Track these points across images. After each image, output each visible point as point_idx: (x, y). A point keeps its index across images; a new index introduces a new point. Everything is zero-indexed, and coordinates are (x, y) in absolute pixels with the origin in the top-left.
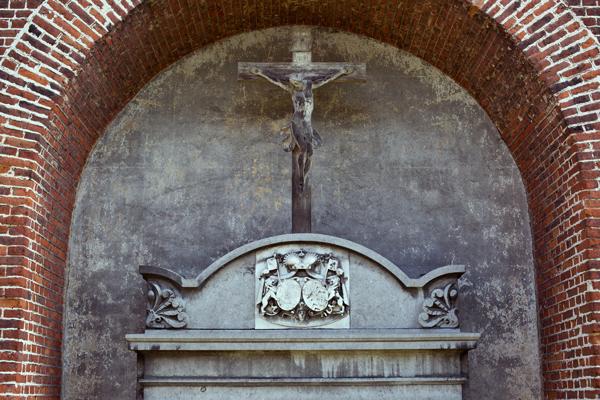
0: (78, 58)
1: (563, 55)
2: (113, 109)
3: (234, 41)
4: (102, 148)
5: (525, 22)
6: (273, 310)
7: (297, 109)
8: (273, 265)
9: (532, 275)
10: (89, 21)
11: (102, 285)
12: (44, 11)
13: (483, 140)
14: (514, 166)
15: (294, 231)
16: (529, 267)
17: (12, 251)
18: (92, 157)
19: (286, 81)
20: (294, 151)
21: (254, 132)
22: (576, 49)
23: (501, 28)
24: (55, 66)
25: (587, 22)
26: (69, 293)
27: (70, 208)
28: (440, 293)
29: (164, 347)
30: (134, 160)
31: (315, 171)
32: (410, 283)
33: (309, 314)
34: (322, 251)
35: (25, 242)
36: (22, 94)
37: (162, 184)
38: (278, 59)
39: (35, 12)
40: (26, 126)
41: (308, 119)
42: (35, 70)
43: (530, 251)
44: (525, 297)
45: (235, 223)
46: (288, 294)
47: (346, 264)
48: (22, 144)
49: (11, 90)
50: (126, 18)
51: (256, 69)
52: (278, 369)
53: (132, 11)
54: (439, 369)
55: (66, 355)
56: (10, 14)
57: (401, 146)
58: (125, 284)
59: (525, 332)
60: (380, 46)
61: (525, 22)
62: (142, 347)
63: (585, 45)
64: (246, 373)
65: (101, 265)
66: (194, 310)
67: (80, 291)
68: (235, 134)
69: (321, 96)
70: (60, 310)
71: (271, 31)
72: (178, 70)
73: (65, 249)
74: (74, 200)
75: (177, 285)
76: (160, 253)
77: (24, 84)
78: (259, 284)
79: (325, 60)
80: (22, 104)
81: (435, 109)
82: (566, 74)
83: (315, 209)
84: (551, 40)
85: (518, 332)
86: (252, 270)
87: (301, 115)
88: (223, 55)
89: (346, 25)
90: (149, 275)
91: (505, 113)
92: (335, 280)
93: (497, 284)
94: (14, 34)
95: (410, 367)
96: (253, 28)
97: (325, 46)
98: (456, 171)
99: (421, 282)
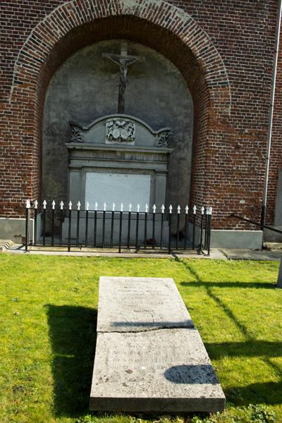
0: (50, 49)
1: (209, 62)
2: (58, 66)
3: (100, 44)
4: (54, 80)
5: (199, 49)
6: (112, 138)
7: (122, 72)
8: (112, 123)
9: (192, 132)
10: (53, 35)
11: (55, 127)
12: (36, 29)
13: (181, 87)
14: (190, 96)
15: (118, 113)
16: (191, 130)
17: (29, 115)
18: (51, 83)
19: (118, 61)
20: (120, 86)
21: (106, 78)
22: (214, 60)
23: (191, 50)
24: (42, 51)
25: (219, 51)
26: (44, 129)
27: (44, 100)
28: (163, 136)
29: (77, 148)
30: (66, 85)
31: (127, 94)
32: (154, 132)
33: (122, 140)
34: (127, 120)
35: (33, 112)
36: (30, 60)
37: (75, 94)
38: (115, 53)
39: (34, 29)
40: (33, 72)
41: (125, 76)
42: (35, 52)
43: (192, 124)
44: (189, 139)
45: (99, 109)
46: (116, 133)
47: (134, 125)
48: (31, 79)
49: (27, 59)
50: (67, 35)
51: (108, 56)
52: (112, 156)
53: (68, 33)
54: (161, 159)
55: (44, 149)
56: (24, 30)
57: (155, 87)
58: (62, 127)
59: (188, 150)
60: (150, 50)
61: (199, 49)
62: (70, 147)
63: (213, 53)
64: (102, 157)
65: (54, 120)
66: (86, 136)
67: (48, 129)
68: (100, 78)
69: (129, 67)
70: (41, 134)
71: (113, 41)
72: (80, 53)
73: (43, 114)
74: (44, 97)
75: (81, 128)
76: (75, 117)
77: (31, 57)
78: (107, 130)
79: (131, 55)
80: (31, 64)
81: (167, 74)
82: (209, 69)
83: (125, 106)
84: (206, 56)
85: (185, 149)
86: (105, 125)
87: (123, 74)
88: (96, 48)
89: (140, 41)
90: (72, 125)
91: (189, 78)
92: (131, 130)
93: (181, 134)
94: (27, 37)
95: (152, 158)
96: (107, 39)
97: (131, 49)
98: (171, 96)
99: (157, 132)
